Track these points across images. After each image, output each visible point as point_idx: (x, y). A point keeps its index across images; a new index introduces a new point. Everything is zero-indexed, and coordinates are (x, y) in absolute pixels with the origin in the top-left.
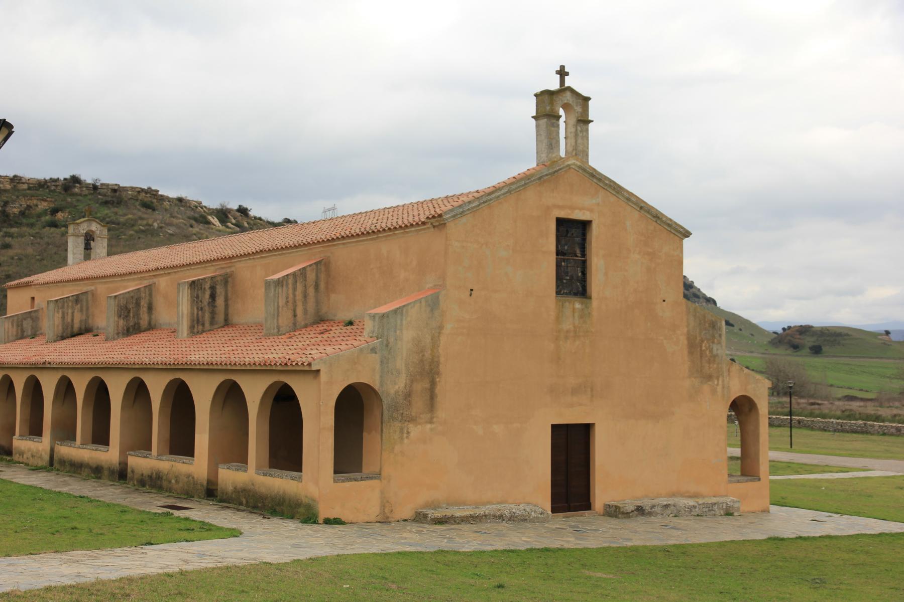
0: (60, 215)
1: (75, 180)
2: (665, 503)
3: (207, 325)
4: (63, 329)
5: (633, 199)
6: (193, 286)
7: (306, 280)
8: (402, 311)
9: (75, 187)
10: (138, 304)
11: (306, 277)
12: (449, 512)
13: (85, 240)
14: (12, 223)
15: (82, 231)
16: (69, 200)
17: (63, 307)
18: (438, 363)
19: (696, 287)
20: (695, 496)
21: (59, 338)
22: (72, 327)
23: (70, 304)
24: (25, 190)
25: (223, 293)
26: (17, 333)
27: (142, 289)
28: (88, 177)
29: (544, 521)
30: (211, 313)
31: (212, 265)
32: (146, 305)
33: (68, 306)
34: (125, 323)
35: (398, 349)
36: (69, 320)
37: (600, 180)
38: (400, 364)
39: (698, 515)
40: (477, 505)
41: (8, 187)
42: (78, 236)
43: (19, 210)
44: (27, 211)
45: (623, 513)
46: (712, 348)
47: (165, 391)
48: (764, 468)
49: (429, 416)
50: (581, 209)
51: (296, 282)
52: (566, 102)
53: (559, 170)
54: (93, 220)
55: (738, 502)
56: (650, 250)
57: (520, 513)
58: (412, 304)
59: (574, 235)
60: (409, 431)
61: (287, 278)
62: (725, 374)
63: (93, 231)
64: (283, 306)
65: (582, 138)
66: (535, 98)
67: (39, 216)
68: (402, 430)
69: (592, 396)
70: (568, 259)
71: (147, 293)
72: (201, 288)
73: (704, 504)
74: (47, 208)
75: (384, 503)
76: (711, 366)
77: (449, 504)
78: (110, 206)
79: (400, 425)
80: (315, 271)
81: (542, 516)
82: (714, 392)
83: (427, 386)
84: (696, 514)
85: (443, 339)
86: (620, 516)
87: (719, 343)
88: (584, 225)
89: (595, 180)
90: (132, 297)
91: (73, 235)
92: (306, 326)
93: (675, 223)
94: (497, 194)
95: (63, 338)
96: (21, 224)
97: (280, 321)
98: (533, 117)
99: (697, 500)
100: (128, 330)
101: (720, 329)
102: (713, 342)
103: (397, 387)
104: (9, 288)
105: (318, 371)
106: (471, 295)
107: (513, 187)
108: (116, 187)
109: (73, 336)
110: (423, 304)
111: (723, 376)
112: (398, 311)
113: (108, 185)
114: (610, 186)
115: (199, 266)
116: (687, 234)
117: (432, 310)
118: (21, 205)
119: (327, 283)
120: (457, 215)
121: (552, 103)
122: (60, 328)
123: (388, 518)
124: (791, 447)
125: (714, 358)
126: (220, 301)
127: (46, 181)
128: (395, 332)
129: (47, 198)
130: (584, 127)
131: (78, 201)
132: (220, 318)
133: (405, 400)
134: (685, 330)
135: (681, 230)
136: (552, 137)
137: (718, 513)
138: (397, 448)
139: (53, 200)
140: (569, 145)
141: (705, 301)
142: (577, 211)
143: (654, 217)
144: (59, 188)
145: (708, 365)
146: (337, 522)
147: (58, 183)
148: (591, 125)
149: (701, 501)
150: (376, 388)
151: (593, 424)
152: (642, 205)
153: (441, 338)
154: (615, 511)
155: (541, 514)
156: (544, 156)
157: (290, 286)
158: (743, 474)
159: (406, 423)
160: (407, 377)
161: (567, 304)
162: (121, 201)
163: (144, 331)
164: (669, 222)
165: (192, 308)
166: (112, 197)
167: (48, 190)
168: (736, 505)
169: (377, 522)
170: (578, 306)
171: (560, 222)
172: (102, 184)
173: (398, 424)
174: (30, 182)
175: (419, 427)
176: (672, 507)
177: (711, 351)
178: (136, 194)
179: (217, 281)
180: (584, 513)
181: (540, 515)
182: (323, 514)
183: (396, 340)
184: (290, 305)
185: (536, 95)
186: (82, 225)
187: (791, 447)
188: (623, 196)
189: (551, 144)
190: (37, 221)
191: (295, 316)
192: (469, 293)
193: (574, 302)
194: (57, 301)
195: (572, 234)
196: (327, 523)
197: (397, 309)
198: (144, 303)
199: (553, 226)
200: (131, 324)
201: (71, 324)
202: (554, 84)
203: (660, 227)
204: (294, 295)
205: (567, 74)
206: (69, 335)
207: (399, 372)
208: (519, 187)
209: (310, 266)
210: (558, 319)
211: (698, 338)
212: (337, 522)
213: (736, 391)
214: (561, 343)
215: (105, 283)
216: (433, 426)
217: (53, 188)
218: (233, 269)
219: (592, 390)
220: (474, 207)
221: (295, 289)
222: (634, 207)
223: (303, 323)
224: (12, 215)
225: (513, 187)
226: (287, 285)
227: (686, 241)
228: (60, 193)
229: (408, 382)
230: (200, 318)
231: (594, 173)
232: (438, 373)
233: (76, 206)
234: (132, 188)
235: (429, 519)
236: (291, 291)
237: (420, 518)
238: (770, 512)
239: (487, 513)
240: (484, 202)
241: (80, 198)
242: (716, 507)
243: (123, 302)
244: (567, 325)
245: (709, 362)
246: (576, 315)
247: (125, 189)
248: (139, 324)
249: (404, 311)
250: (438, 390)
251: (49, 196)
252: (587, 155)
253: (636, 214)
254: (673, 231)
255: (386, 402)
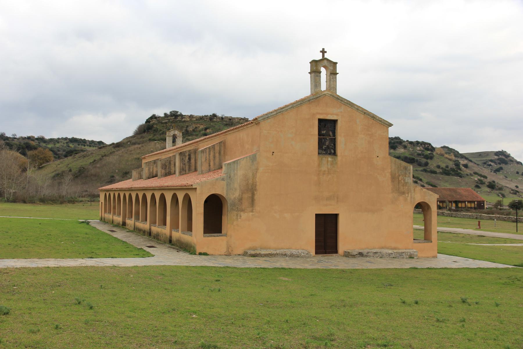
0: (208, 131)
1: (214, 115)
2: (375, 251)
3: (187, 171)
4: (149, 174)
5: (360, 109)
6: (181, 155)
7: (215, 150)
8: (238, 162)
9: (214, 118)
10: (170, 163)
11: (215, 149)
12: (258, 252)
13: (173, 138)
14: (190, 134)
15: (171, 134)
16: (212, 124)
17: (149, 165)
18: (256, 185)
19: (511, 157)
20: (395, 248)
21: (147, 178)
22: (153, 173)
23: (152, 164)
24: (195, 121)
25: (194, 157)
26: (139, 177)
27: (172, 157)
28: (219, 115)
29: (310, 257)
30: (189, 166)
31: (193, 146)
32: (173, 164)
33: (151, 165)
34: (165, 171)
35: (235, 179)
36: (152, 171)
37: (342, 101)
38: (236, 185)
39: (394, 258)
40: (276, 249)
41: (188, 120)
42: (170, 136)
43: (192, 129)
44: (195, 130)
45: (351, 255)
46: (405, 179)
47: (160, 199)
48: (434, 236)
49: (251, 209)
50: (331, 114)
51: (210, 151)
52: (324, 65)
53: (319, 97)
54: (176, 130)
55: (417, 252)
56: (370, 133)
57: (295, 254)
58: (243, 159)
59: (329, 127)
60: (241, 215)
61: (206, 149)
62: (412, 191)
63: (176, 134)
64: (204, 162)
65: (333, 81)
66: (310, 64)
67: (200, 131)
68: (237, 215)
69: (338, 201)
70: (325, 138)
71: (174, 158)
72: (184, 155)
73: (397, 252)
74: (203, 128)
75: (228, 247)
76: (404, 187)
77: (261, 248)
78: (228, 126)
79: (236, 212)
80: (219, 146)
81: (307, 255)
82: (406, 200)
83: (250, 195)
84: (392, 257)
85: (258, 175)
86: (350, 256)
87: (409, 177)
88: (334, 122)
89: (339, 101)
90: (167, 160)
91: (168, 136)
92: (215, 170)
93: (384, 120)
94: (286, 108)
95: (149, 178)
96: (193, 135)
97: (203, 168)
98: (309, 73)
99: (393, 250)
100: (166, 174)
101: (409, 170)
102: (405, 176)
103: (235, 196)
104: (143, 159)
105: (196, 188)
106: (273, 155)
107: (295, 105)
108: (231, 118)
109: (153, 177)
110: (248, 158)
111: (411, 193)
112: (236, 162)
113: (227, 117)
114: (347, 103)
115: (189, 146)
116: (391, 125)
117: (253, 162)
118: (193, 127)
119: (224, 151)
120: (265, 118)
121: (316, 66)
122: (148, 174)
123: (230, 253)
124: (517, 232)
125: (406, 184)
126: (193, 161)
127: (203, 116)
128: (234, 171)
129: (203, 123)
130: (334, 76)
131: (215, 124)
132: (193, 168)
133: (239, 201)
134: (390, 171)
135: (387, 123)
136: (317, 82)
137: (405, 257)
138: (235, 223)
139: (205, 124)
140: (327, 85)
141: (516, 163)
142: (329, 115)
143: (372, 117)
144: (208, 119)
145: (403, 187)
146: (205, 254)
147: (207, 117)
148: (338, 75)
149: (395, 251)
150: (224, 196)
151: (339, 214)
152: (365, 112)
153: (257, 174)
154: (348, 254)
155: (307, 254)
156: (313, 90)
157: (207, 153)
158: (425, 240)
159: (240, 212)
160: (240, 191)
161: (324, 158)
162: (233, 124)
163: (173, 174)
164: (380, 119)
165: (180, 164)
166: (229, 122)
167: (203, 120)
168: (415, 253)
169: (225, 255)
170: (330, 159)
171: (320, 121)
172: (225, 117)
173: (235, 213)
174: (197, 117)
175: (246, 213)
176: (379, 253)
177: (404, 180)
178: (239, 120)
179: (192, 152)
180: (333, 255)
181: (306, 255)
182: (198, 250)
183: (234, 175)
184: (207, 161)
185: (310, 63)
186: (171, 132)
187: (517, 232)
188: (355, 108)
189: (316, 85)
190: (199, 133)
191: (210, 166)
192: (272, 154)
193: (328, 158)
194: (146, 163)
195: (328, 126)
196: (200, 255)
197: (235, 161)
198: (172, 163)
199: (316, 123)
200: (167, 171)
201: (152, 172)
202: (319, 57)
203: (376, 122)
204: (209, 157)
205: (326, 52)
206: (151, 177)
207: (236, 189)
208: (297, 105)
209: (217, 144)
210: (319, 165)
211: (397, 175)
212: (205, 254)
213: (418, 199)
214: (321, 176)
215: (165, 155)
216: (253, 214)
217: (206, 119)
218: (198, 147)
219: (337, 198)
220: (274, 115)
221: (209, 154)
222: (361, 113)
223: (213, 169)
224: (190, 131)
225: (295, 105)
226: (206, 152)
227: (390, 128)
228: (208, 121)
229: (240, 193)
230: (184, 168)
231: (339, 98)
232: (256, 190)
233: (214, 126)
234: (237, 118)
235: (248, 254)
236: (207, 155)
237: (245, 254)
238: (438, 257)
239: (278, 253)
240: (279, 112)
241: (216, 123)
242: (404, 254)
243: (163, 162)
244: (324, 168)
245: (403, 186)
246: (329, 163)
247: (234, 118)
248: (170, 171)
249: (239, 162)
250: (256, 197)
251: (204, 123)
252: (336, 89)
253: (362, 116)
254: (382, 124)
255: (229, 202)
